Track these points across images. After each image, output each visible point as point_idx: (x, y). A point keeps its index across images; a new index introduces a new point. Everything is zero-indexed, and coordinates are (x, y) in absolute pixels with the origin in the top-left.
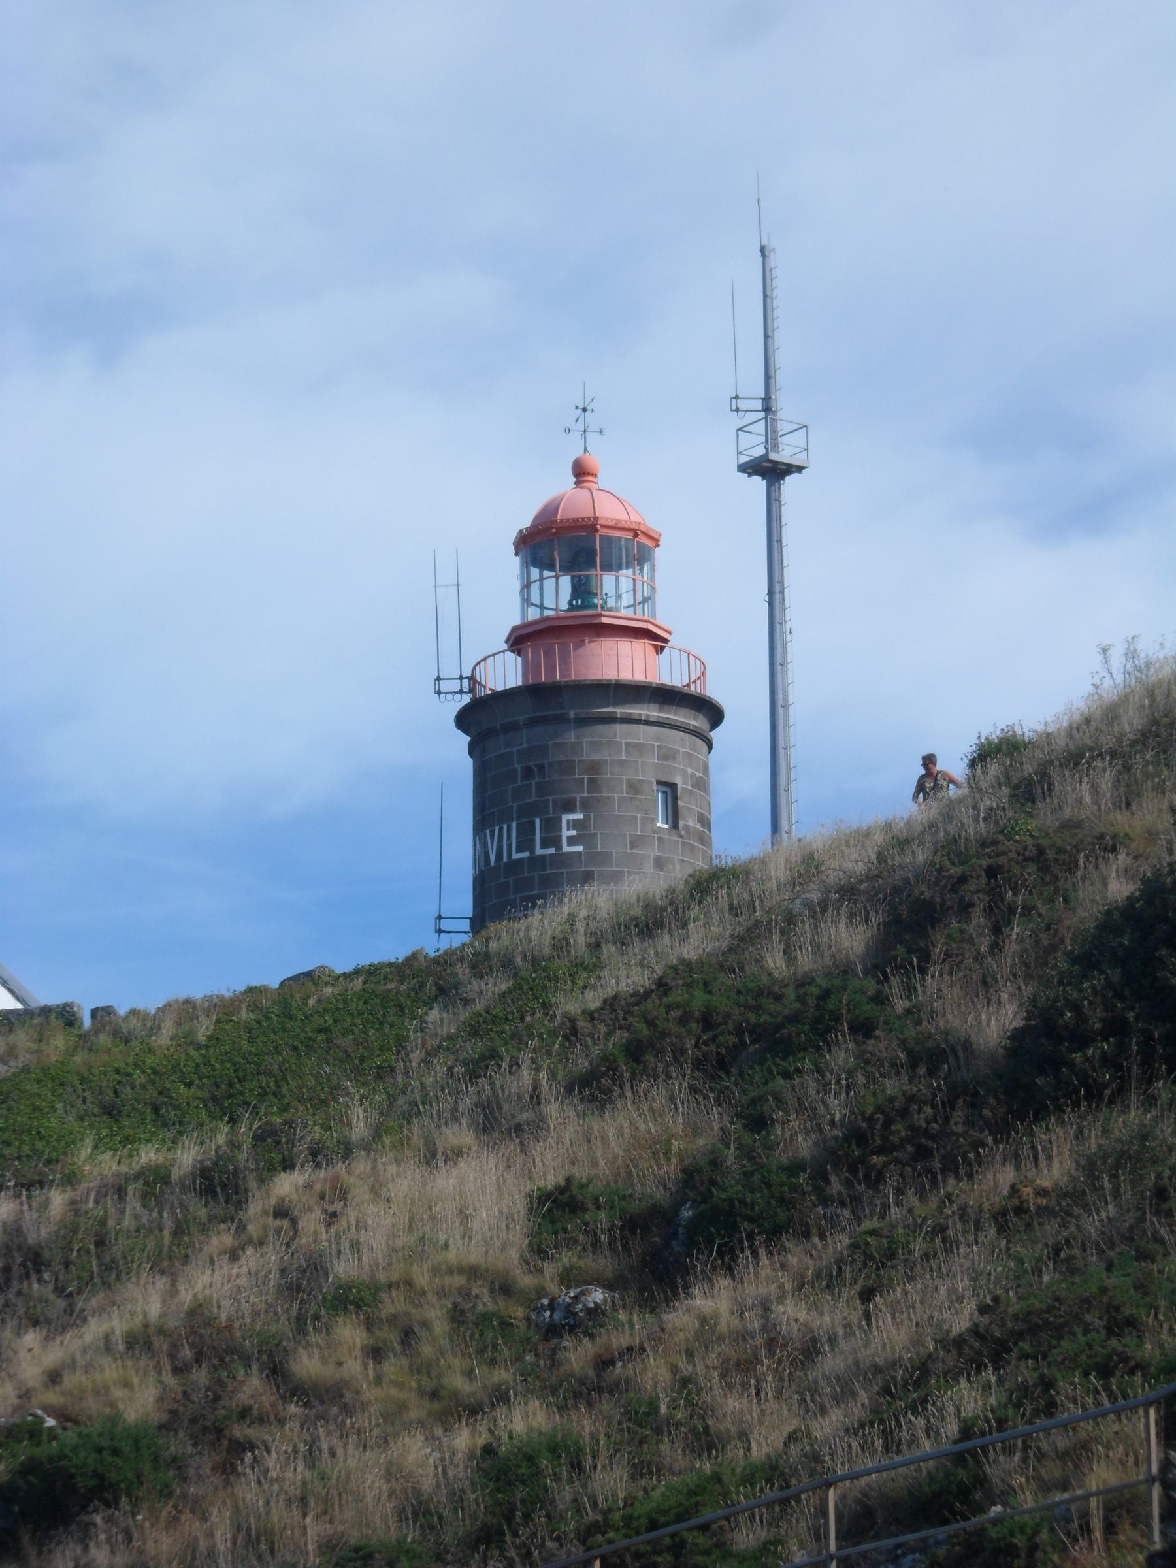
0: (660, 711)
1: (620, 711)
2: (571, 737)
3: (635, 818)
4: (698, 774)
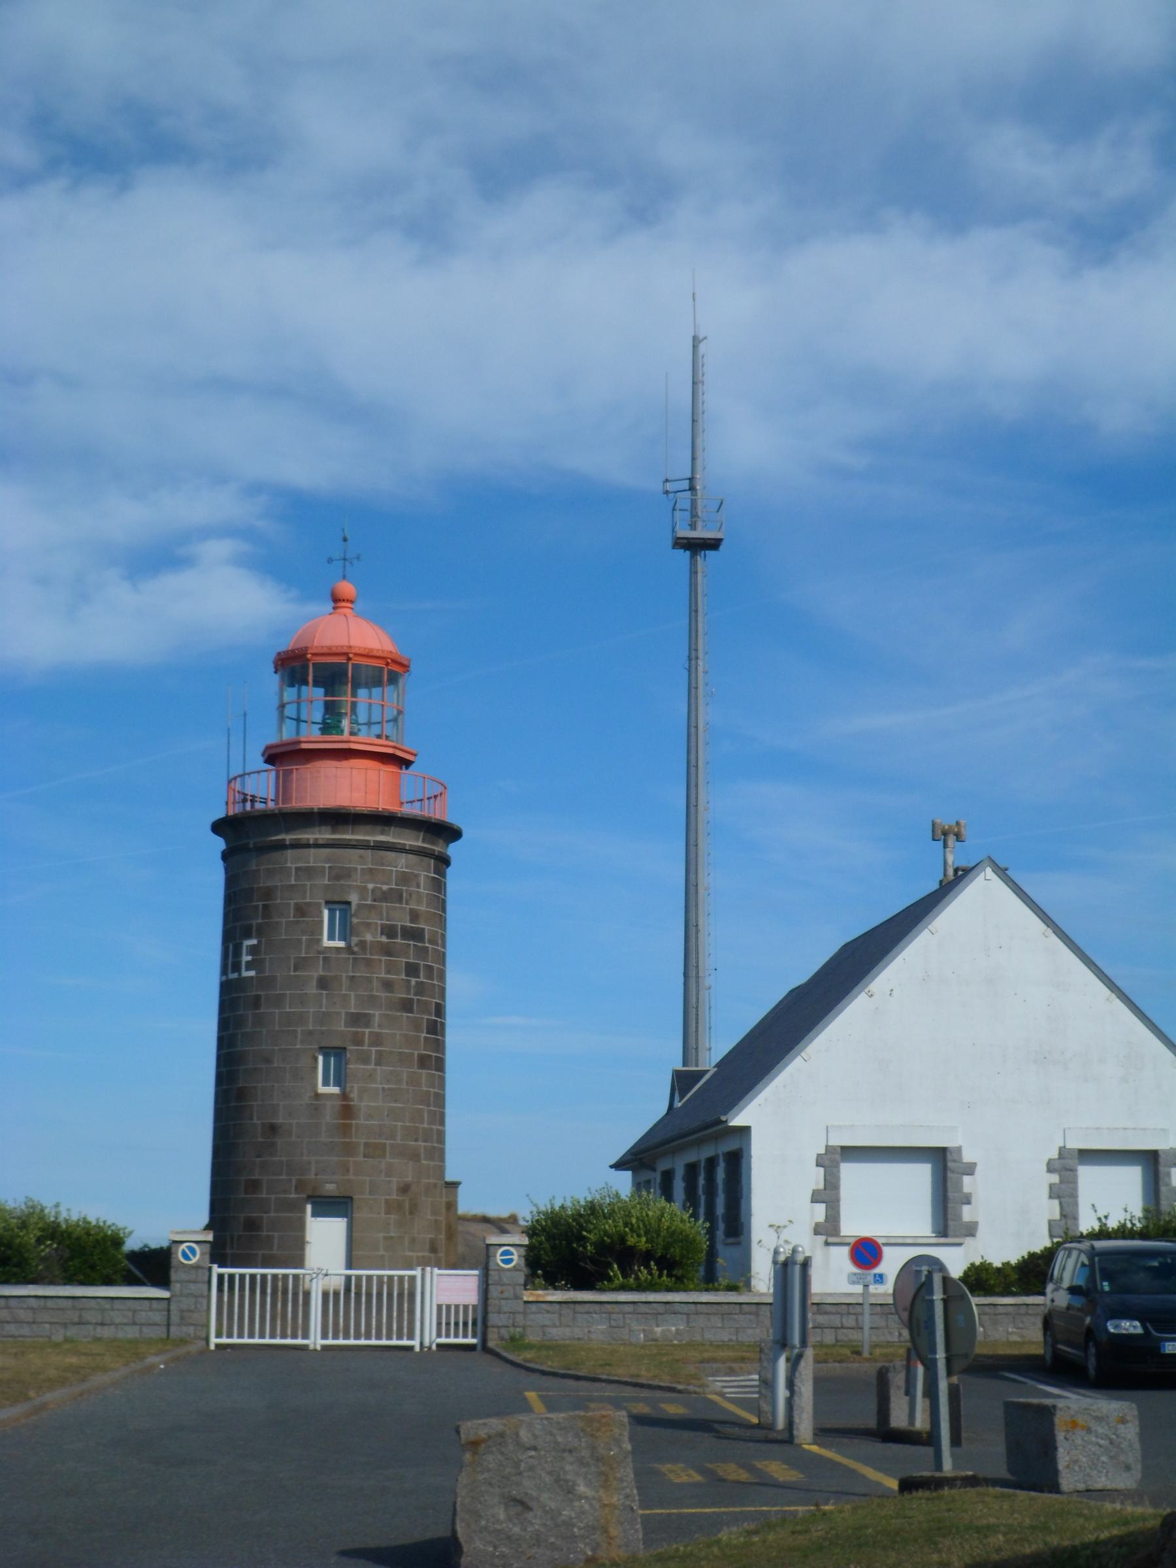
0: (334, 832)
1: (288, 837)
3: (300, 941)
4: (385, 887)
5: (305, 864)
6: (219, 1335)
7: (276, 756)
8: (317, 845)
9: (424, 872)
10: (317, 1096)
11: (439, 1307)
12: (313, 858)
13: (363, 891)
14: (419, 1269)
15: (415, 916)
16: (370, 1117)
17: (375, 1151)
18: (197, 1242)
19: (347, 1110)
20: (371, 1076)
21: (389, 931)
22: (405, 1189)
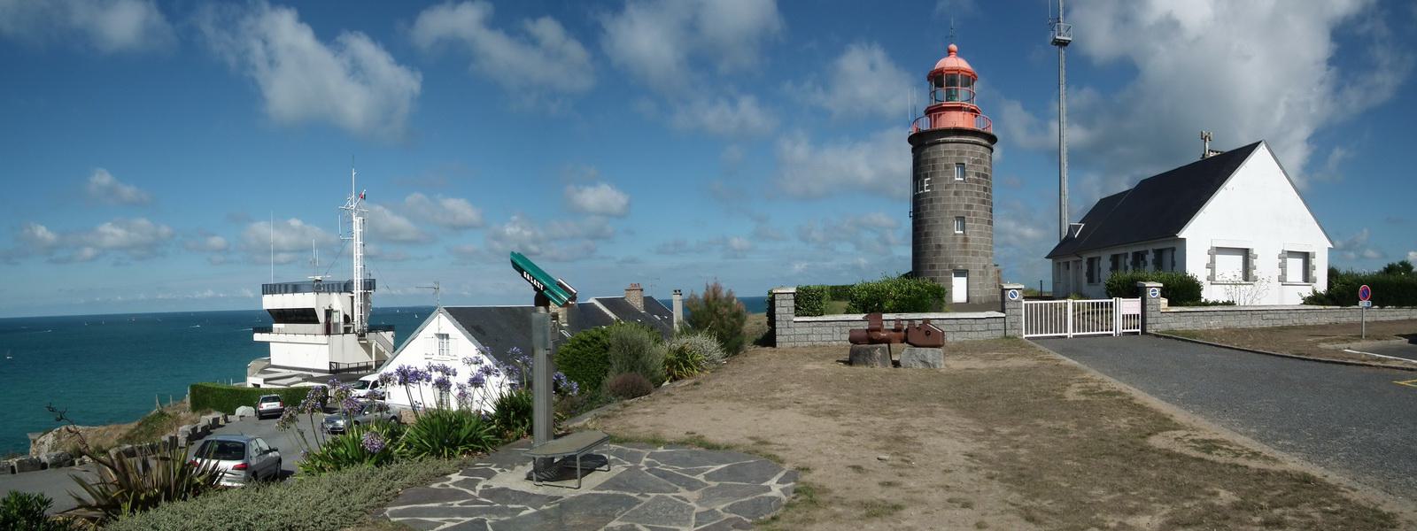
2: (927, 150)
5: (947, 152)
7: (929, 112)
8: (952, 142)
11: (1123, 316)
13: (969, 159)
16: (973, 242)
17: (975, 254)
19: (966, 240)
20: (973, 227)
21: (978, 174)
22: (985, 267)
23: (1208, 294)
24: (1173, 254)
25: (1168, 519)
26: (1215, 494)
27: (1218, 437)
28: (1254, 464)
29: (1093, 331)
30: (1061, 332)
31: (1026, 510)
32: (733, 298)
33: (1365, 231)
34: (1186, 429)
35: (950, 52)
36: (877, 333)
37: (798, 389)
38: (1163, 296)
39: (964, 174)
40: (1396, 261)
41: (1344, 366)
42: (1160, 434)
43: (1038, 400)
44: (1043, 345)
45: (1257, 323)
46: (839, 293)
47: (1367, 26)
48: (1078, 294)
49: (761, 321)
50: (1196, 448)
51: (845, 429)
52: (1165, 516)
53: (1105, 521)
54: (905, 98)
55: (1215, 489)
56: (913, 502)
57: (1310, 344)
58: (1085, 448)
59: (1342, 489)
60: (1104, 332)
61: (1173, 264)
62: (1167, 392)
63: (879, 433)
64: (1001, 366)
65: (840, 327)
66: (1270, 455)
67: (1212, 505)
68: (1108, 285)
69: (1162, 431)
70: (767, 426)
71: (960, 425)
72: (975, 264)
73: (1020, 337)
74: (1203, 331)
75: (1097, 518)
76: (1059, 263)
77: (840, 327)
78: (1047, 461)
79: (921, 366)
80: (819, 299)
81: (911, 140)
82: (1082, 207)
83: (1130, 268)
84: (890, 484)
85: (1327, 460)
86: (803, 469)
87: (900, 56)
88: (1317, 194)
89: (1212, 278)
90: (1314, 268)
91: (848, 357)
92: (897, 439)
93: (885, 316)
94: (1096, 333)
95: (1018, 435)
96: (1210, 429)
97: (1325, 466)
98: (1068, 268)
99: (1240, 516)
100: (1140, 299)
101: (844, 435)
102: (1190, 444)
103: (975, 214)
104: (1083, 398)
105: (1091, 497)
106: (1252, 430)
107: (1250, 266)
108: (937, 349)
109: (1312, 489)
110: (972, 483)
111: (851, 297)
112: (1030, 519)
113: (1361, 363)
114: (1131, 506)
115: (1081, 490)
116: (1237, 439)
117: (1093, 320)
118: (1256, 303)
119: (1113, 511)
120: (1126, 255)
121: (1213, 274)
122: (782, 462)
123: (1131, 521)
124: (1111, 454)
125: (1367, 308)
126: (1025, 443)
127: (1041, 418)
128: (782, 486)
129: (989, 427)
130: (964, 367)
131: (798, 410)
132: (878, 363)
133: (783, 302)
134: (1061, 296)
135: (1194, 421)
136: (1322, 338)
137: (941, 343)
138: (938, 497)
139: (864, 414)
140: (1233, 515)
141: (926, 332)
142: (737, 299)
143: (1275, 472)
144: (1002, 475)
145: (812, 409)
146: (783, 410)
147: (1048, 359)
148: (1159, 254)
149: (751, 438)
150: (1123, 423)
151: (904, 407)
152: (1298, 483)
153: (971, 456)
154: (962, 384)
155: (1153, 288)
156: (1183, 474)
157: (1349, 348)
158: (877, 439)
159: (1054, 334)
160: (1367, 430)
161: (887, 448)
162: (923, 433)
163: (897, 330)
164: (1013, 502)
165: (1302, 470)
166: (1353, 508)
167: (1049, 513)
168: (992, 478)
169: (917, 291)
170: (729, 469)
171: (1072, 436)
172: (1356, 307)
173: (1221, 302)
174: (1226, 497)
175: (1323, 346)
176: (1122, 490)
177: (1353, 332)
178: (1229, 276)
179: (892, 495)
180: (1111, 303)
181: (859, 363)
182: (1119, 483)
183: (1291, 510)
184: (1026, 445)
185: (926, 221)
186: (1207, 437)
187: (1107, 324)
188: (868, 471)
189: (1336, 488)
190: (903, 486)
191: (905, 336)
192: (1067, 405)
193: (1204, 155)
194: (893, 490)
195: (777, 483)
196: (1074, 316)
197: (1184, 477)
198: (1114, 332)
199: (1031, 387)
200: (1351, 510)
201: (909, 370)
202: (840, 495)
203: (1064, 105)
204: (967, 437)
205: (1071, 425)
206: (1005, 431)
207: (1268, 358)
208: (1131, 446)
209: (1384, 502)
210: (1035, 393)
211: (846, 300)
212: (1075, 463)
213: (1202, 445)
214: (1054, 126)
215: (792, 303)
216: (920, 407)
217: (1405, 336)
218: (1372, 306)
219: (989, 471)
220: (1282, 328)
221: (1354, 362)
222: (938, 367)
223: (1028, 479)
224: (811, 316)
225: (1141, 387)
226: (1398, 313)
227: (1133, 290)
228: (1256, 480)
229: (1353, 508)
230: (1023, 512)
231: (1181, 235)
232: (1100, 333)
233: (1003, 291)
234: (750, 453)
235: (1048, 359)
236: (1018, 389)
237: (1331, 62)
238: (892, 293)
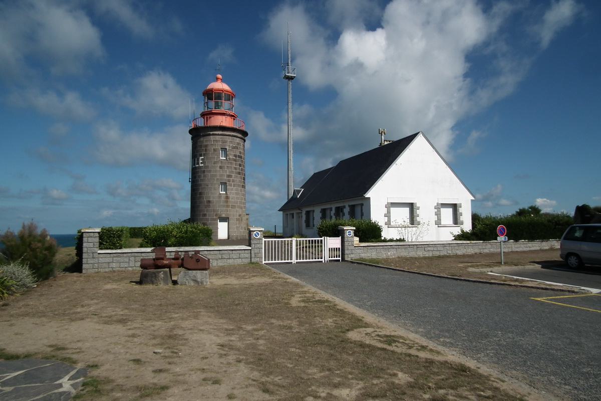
1: (217, 133)
2: (202, 139)
5: (214, 141)
6: (265, 260)
7: (203, 115)
8: (218, 135)
9: (241, 142)
10: (220, 194)
11: (329, 248)
12: (217, 138)
14: (323, 237)
15: (240, 153)
16: (232, 199)
17: (233, 207)
18: (259, 231)
19: (227, 198)
20: (232, 189)
21: (235, 156)
22: (240, 215)
23: (386, 234)
24: (362, 208)
25: (362, 392)
26: (395, 375)
27: (396, 334)
28: (423, 355)
29: (309, 259)
30: (288, 260)
31: (263, 384)
32: (47, 235)
33: (499, 186)
34: (373, 327)
35: (217, 79)
36: (162, 261)
37: (96, 304)
38: (356, 235)
39: (226, 156)
40: (526, 206)
41: (488, 285)
42: (355, 330)
43: (272, 306)
44: (275, 268)
45: (421, 253)
46: (136, 233)
47: (492, 48)
48: (299, 234)
49: (71, 253)
50: (380, 341)
51: (130, 332)
52: (360, 389)
53: (318, 392)
54: (188, 108)
55: (395, 372)
56: (177, 382)
57: (461, 269)
58: (304, 339)
59: (493, 379)
60: (317, 260)
61: (362, 215)
62: (359, 301)
63: (156, 333)
64: (247, 282)
65: (135, 257)
66: (434, 349)
67: (393, 383)
68: (319, 228)
69: (357, 328)
70: (66, 335)
71: (217, 325)
72: (233, 213)
73: (261, 263)
74: (383, 259)
75: (312, 389)
76: (288, 214)
77: (135, 257)
78: (278, 348)
79: (192, 284)
80: (119, 237)
81: (191, 132)
82: (302, 178)
83: (334, 217)
84: (161, 371)
85: (479, 355)
86: (92, 366)
87: (183, 80)
88: (460, 163)
89: (388, 224)
90: (461, 214)
91: (139, 278)
92: (170, 337)
93: (168, 249)
94: (311, 260)
95: (259, 330)
96: (391, 328)
97: (478, 359)
98: (293, 217)
99: (413, 392)
100: (340, 238)
101: (129, 337)
102: (376, 338)
103: (233, 181)
104: (303, 304)
105: (308, 375)
106: (420, 330)
107: (415, 215)
108: (204, 272)
109: (468, 376)
110: (222, 365)
111: (145, 237)
112: (266, 391)
113: (502, 282)
114: (335, 381)
115: (301, 369)
116: (410, 335)
117: (309, 252)
118: (420, 240)
119: (323, 384)
120: (331, 209)
121: (389, 220)
122: (75, 362)
123: (336, 392)
124: (322, 344)
125: (504, 242)
126: (263, 336)
127: (274, 318)
128: (72, 382)
129: (239, 325)
130: (223, 283)
131: (95, 320)
132: (162, 282)
133: (89, 239)
134: (288, 235)
135: (379, 321)
136: (469, 264)
137: (207, 267)
138: (196, 377)
139: (147, 320)
140: (408, 392)
141: (197, 262)
142: (51, 236)
143: (439, 362)
144: (247, 359)
145: (106, 319)
146: (82, 321)
147: (279, 278)
148: (353, 208)
149: (50, 346)
150: (330, 322)
151: (177, 313)
152: (457, 372)
153: (223, 346)
154: (220, 295)
155: (349, 230)
156: (373, 359)
157: (491, 272)
158: (155, 337)
159: (283, 261)
160: (510, 335)
161: (161, 344)
162: (190, 331)
163: (176, 259)
164: (254, 378)
165: (459, 361)
166: (502, 395)
167: (279, 386)
168: (239, 361)
169: (192, 232)
170: (25, 374)
171: (295, 331)
172: (496, 241)
173: (395, 239)
174: (403, 378)
175: (471, 270)
176: (329, 370)
177: (494, 260)
178: (400, 222)
179: (162, 379)
180: (321, 240)
181: (147, 283)
182: (327, 364)
183: (452, 391)
184: (264, 337)
185: (200, 185)
186: (388, 334)
187: (318, 254)
188: (145, 362)
189: (487, 378)
190: (171, 372)
191: (182, 263)
192: (291, 309)
193: (381, 144)
194: (163, 375)
195: (69, 380)
196: (297, 249)
197: (372, 361)
198: (323, 260)
199: (268, 297)
200: (501, 397)
201: (183, 287)
202: (121, 383)
203: (291, 115)
204: (221, 333)
205: (294, 323)
206: (249, 328)
207: (431, 277)
208: (335, 338)
209: (529, 394)
210: (270, 301)
211: (141, 237)
212: (297, 350)
213: (385, 339)
214: (285, 127)
215: (97, 240)
216: (190, 313)
217: (538, 263)
218: (509, 240)
219: (237, 356)
220: (439, 257)
221: (496, 282)
222: (205, 284)
223: (265, 362)
224: (112, 249)
225: (342, 298)
226: (530, 245)
227: (336, 232)
228: (424, 366)
229: (502, 395)
230: (261, 385)
231: (367, 195)
232: (314, 260)
233: (250, 232)
234: (47, 358)
235: (279, 278)
236: (259, 298)
237: (466, 75)
238: (174, 233)
